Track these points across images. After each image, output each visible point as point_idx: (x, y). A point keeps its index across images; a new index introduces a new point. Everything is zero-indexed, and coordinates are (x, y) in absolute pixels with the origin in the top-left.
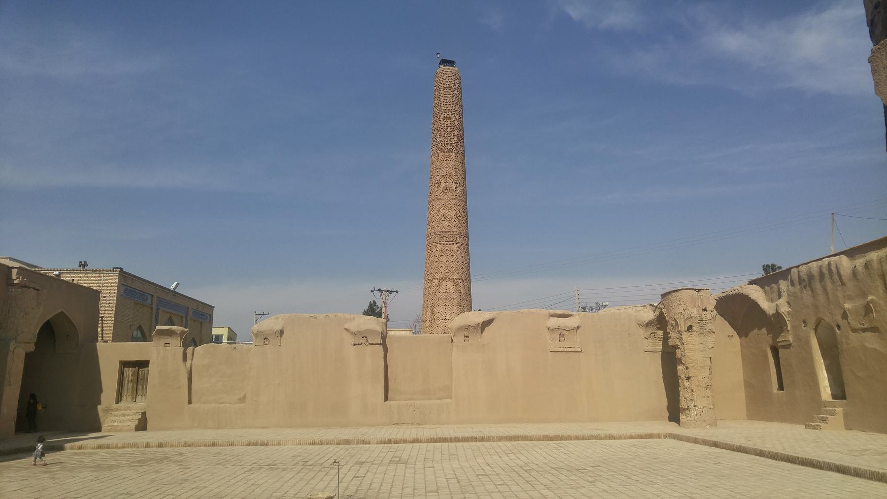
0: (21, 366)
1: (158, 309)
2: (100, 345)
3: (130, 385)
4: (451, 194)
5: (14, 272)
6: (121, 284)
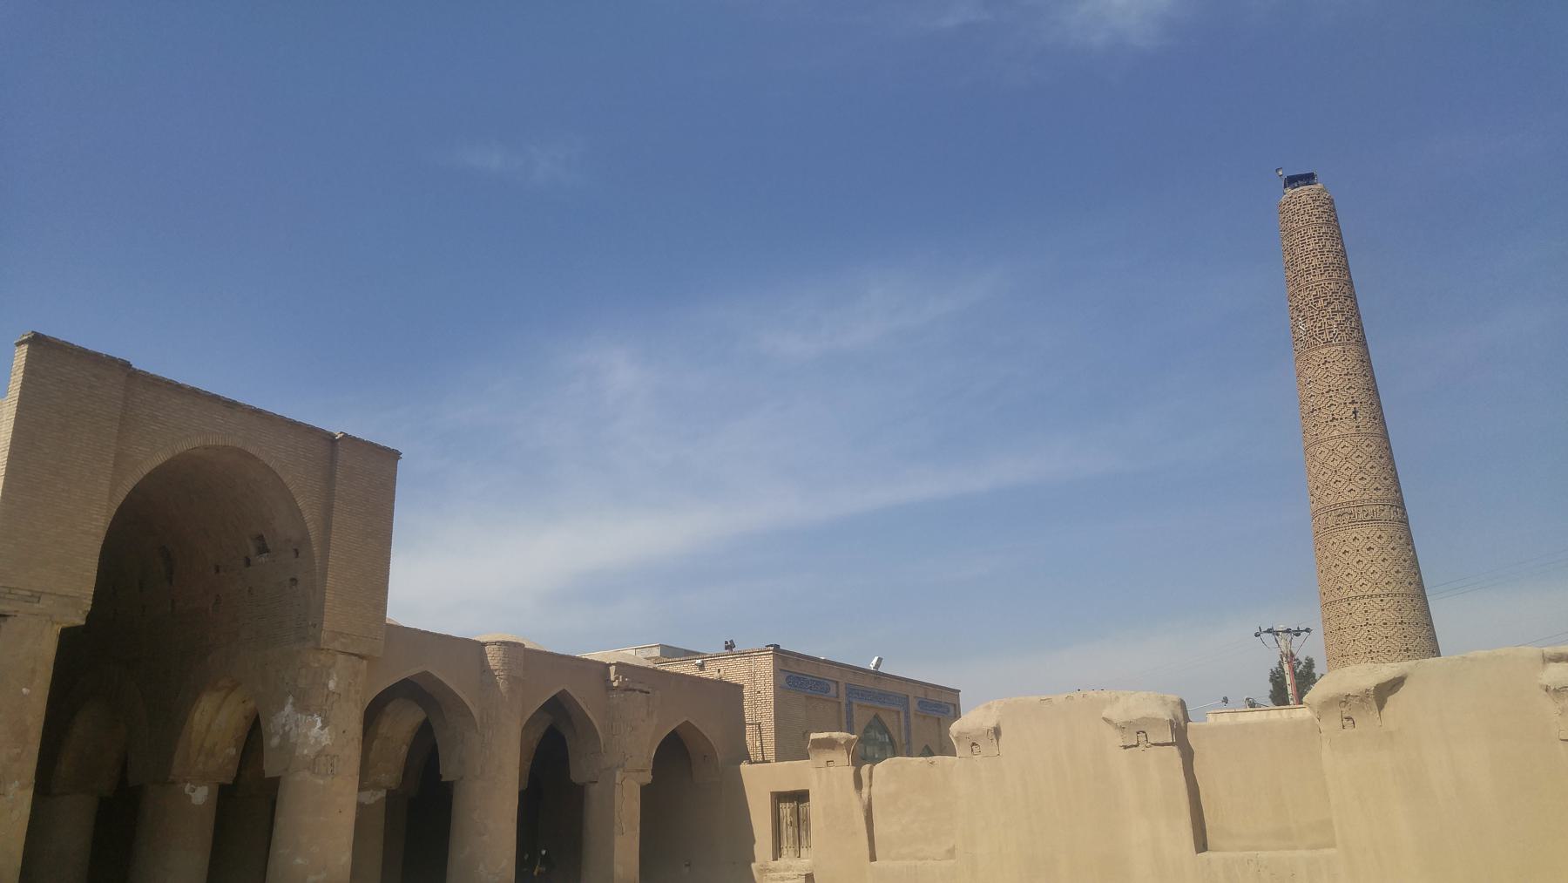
0: (636, 806)
1: (850, 704)
2: (745, 767)
3: (790, 830)
4: (1347, 427)
5: (612, 669)
6: (778, 672)
